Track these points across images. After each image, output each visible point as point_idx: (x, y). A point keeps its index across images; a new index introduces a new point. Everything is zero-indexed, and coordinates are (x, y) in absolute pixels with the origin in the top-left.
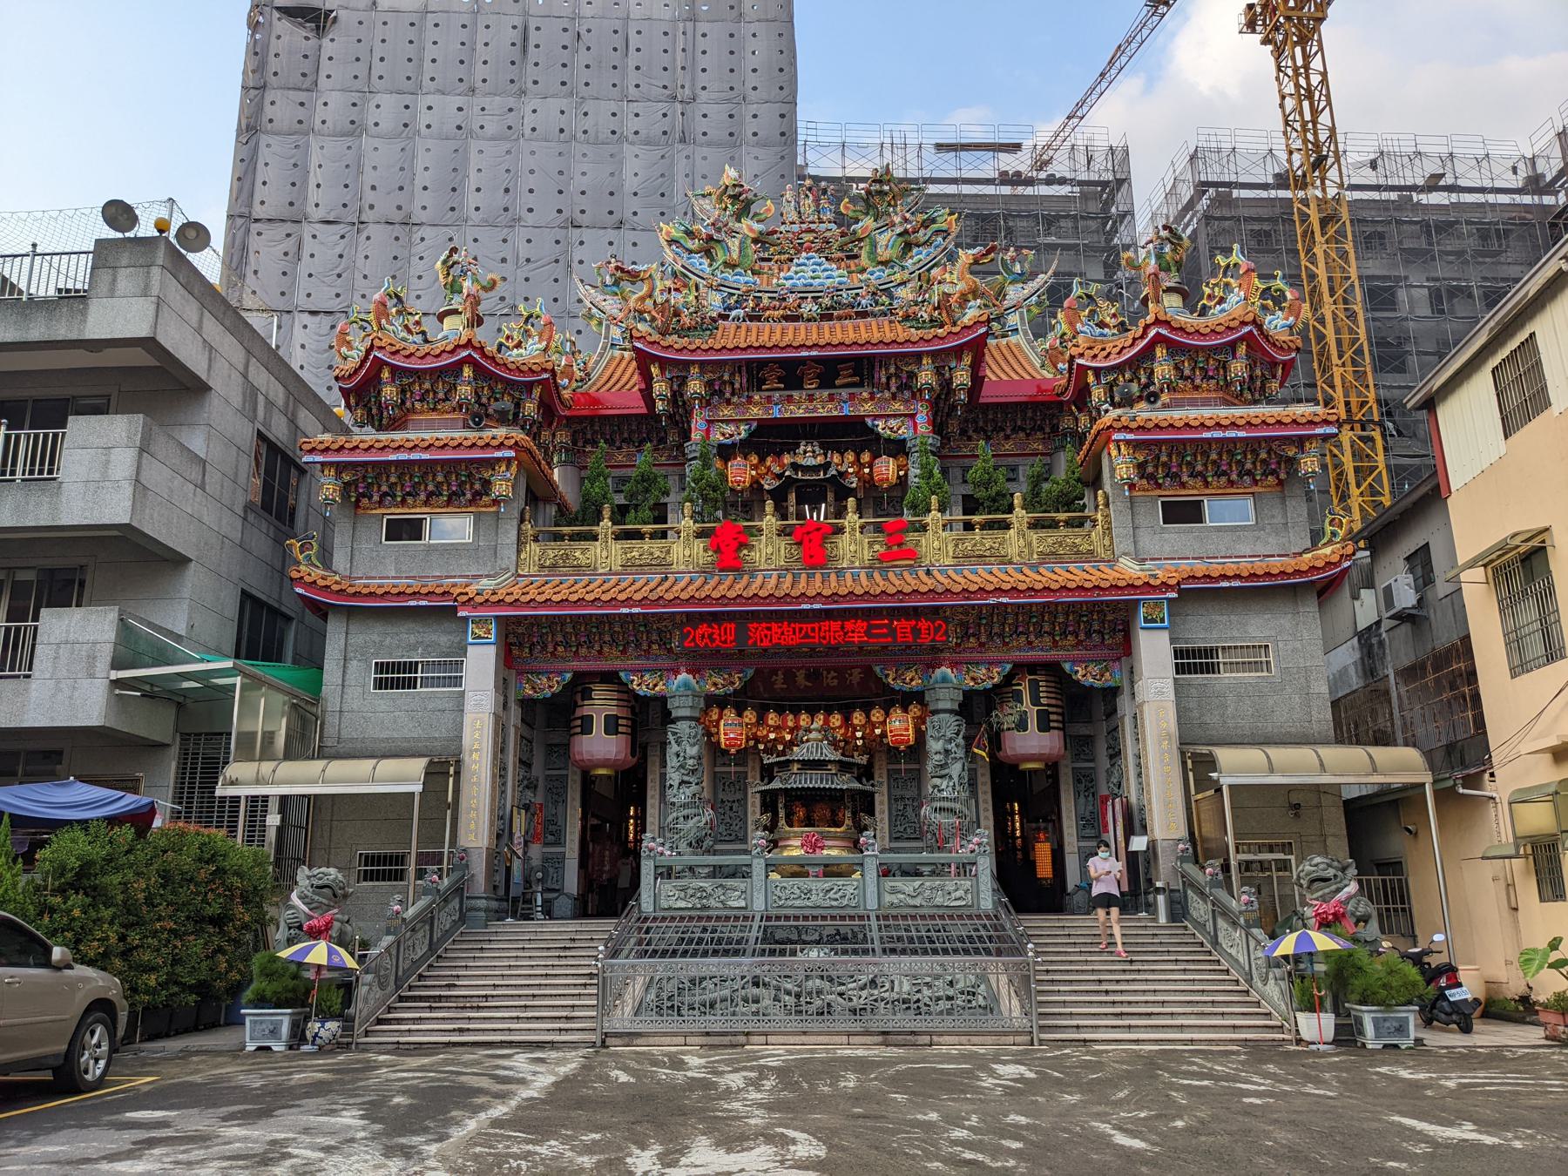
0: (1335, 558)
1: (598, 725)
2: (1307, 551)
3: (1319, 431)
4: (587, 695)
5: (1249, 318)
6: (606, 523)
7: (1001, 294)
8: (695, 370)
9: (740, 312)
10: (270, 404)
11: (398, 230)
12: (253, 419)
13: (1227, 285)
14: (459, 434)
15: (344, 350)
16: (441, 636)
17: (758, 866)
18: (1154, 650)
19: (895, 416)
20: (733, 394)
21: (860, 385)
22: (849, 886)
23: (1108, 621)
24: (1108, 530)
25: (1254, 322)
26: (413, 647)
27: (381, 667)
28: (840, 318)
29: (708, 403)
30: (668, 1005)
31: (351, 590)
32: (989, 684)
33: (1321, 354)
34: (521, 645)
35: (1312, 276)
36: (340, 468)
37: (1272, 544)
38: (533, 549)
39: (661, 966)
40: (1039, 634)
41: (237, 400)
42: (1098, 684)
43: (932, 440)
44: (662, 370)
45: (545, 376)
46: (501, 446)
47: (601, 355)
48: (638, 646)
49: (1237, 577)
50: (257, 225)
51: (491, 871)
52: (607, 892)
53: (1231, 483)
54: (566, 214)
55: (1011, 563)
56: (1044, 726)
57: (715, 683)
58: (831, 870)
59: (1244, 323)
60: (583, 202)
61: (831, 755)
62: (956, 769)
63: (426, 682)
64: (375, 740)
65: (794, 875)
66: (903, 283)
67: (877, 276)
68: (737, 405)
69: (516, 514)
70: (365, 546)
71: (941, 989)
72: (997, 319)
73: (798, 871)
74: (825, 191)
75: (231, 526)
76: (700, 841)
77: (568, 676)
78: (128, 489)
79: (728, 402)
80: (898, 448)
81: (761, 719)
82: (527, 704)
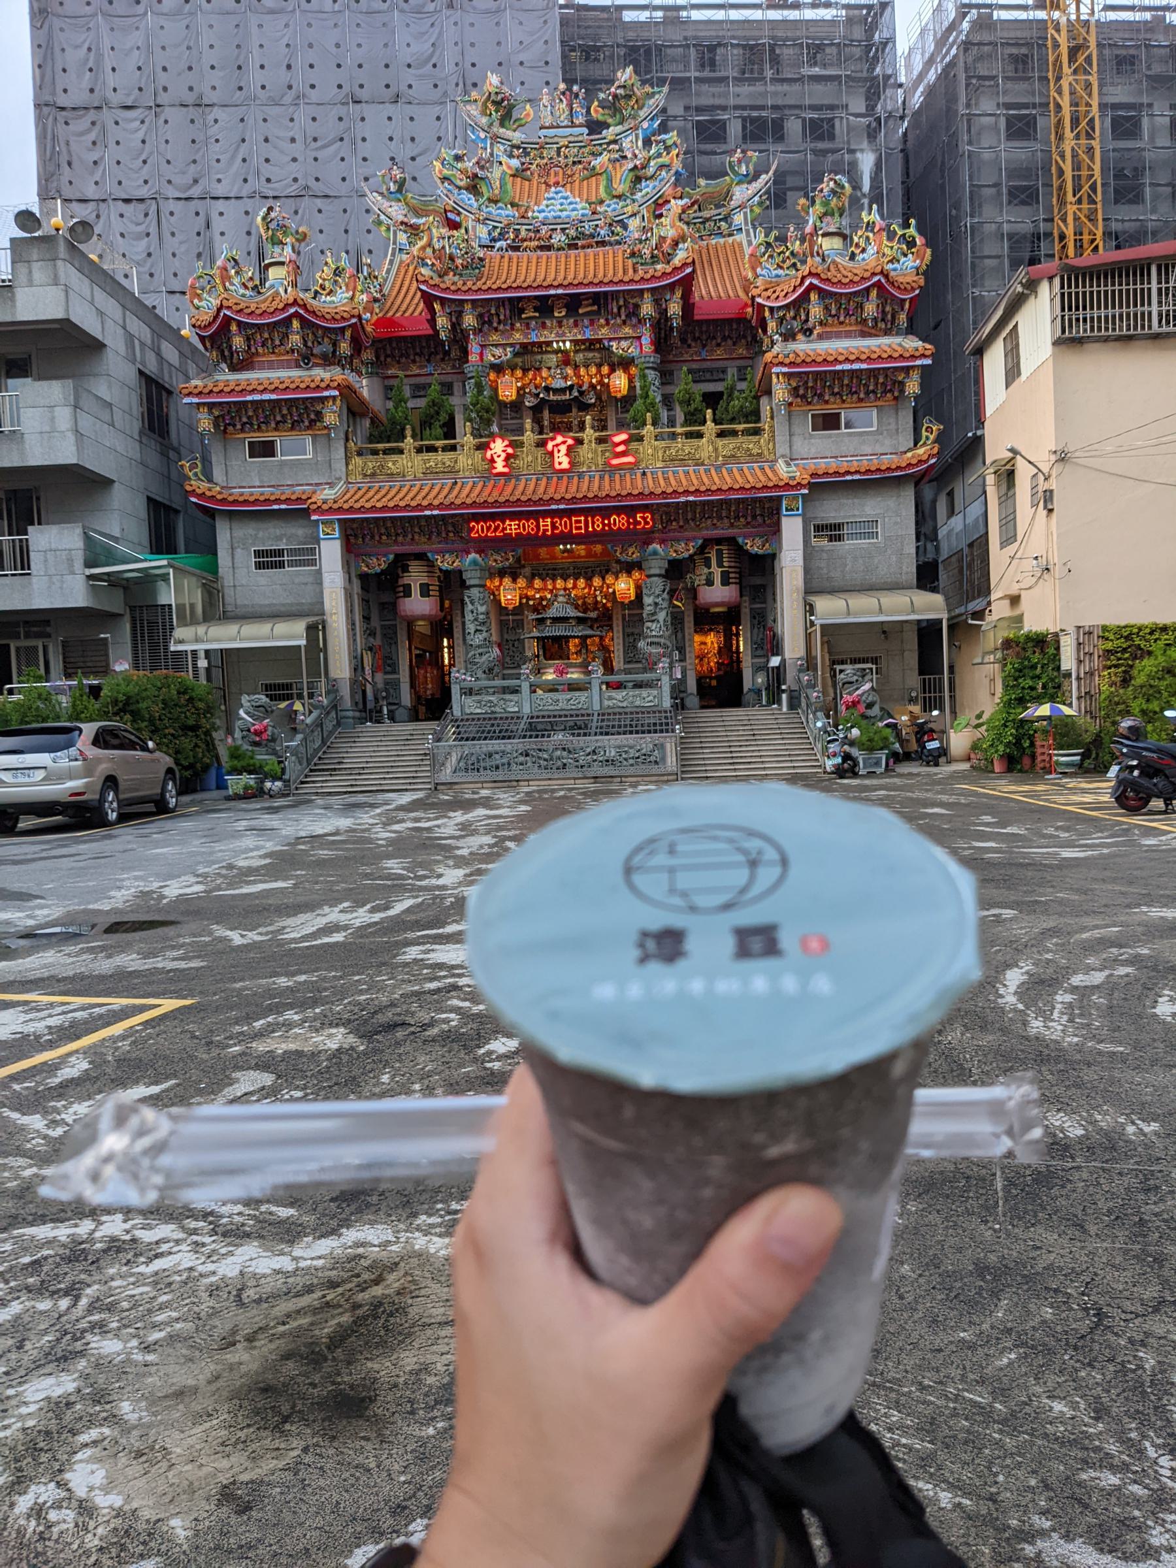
0: (925, 457)
1: (416, 591)
2: (910, 450)
3: (918, 362)
4: (405, 569)
5: (878, 269)
6: (409, 440)
7: (728, 195)
8: (468, 307)
9: (502, 244)
10: (142, 344)
11: (192, 112)
12: (134, 362)
13: (868, 238)
14: (295, 373)
15: (196, 301)
16: (298, 531)
17: (525, 687)
18: (792, 529)
19: (626, 338)
20: (499, 322)
21: (598, 313)
22: (582, 696)
23: (763, 510)
24: (773, 438)
25: (882, 272)
26: (279, 538)
27: (258, 554)
28: (583, 247)
29: (480, 331)
30: (472, 766)
31: (231, 499)
32: (686, 555)
33: (1060, 188)
34: (356, 536)
35: (1058, 107)
36: (211, 406)
37: (887, 445)
38: (358, 461)
39: (469, 747)
40: (720, 518)
41: (122, 349)
42: (761, 552)
43: (654, 359)
44: (442, 305)
45: (354, 321)
46: (328, 387)
47: (391, 262)
48: (439, 534)
49: (857, 472)
50: (64, 113)
51: (353, 693)
52: (433, 705)
53: (860, 400)
54: (346, 89)
55: (703, 464)
56: (725, 582)
57: (496, 560)
58: (573, 687)
59: (874, 274)
60: (361, 76)
61: (572, 613)
62: (662, 616)
63: (292, 564)
64: (261, 606)
65: (551, 691)
66: (634, 215)
67: (611, 208)
68: (503, 332)
69: (342, 436)
70: (235, 463)
71: (632, 753)
72: (725, 219)
73: (552, 688)
74: (577, 96)
75: (132, 449)
76: (491, 670)
77: (391, 557)
78: (71, 437)
79: (496, 329)
80: (625, 363)
81: (530, 585)
82: (363, 577)
